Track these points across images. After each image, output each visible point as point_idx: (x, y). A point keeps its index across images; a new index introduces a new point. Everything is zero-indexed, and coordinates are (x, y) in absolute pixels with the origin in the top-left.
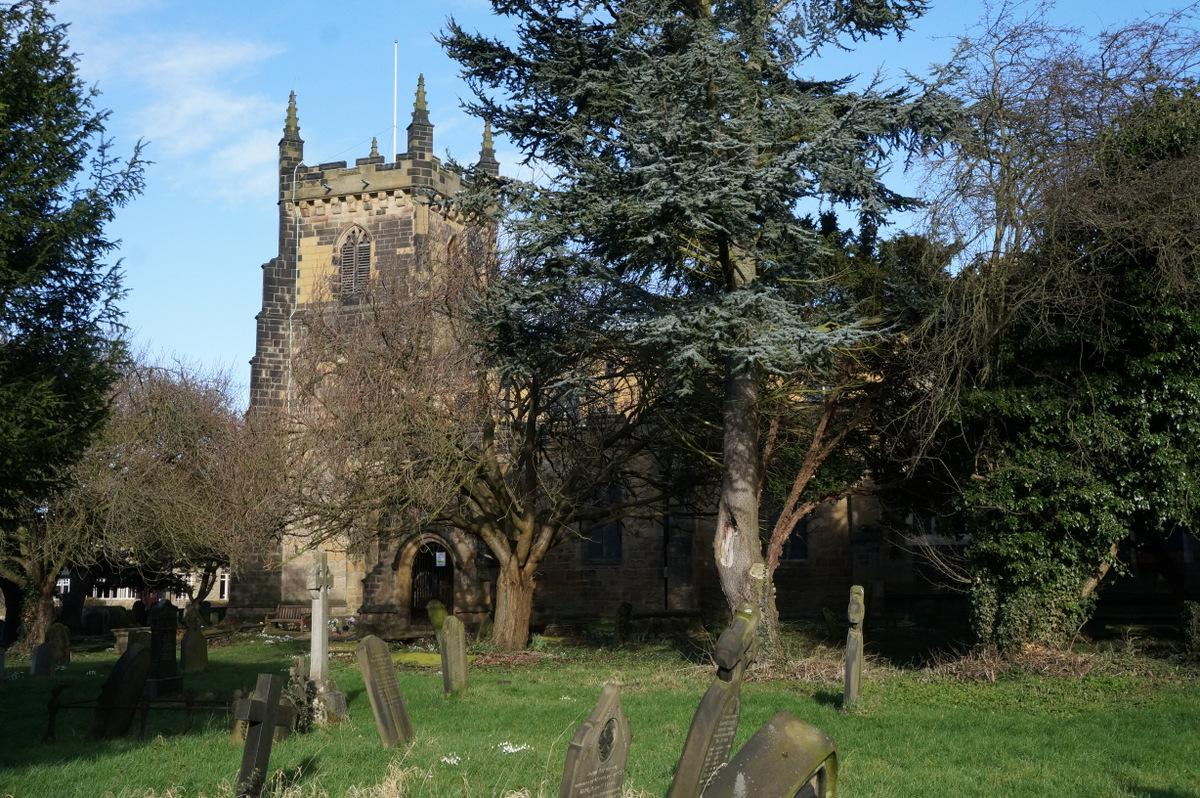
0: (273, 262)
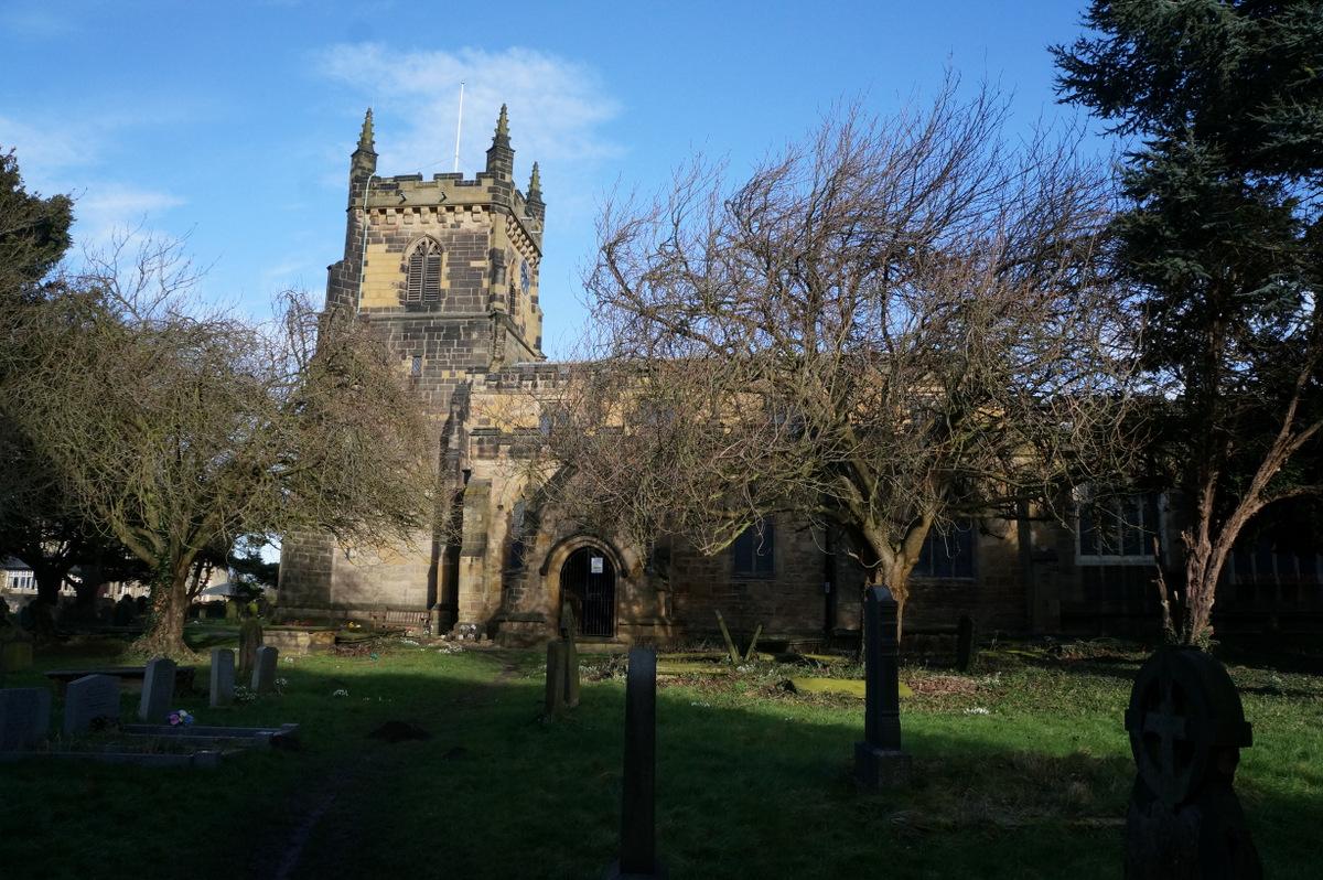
0: (339, 264)
